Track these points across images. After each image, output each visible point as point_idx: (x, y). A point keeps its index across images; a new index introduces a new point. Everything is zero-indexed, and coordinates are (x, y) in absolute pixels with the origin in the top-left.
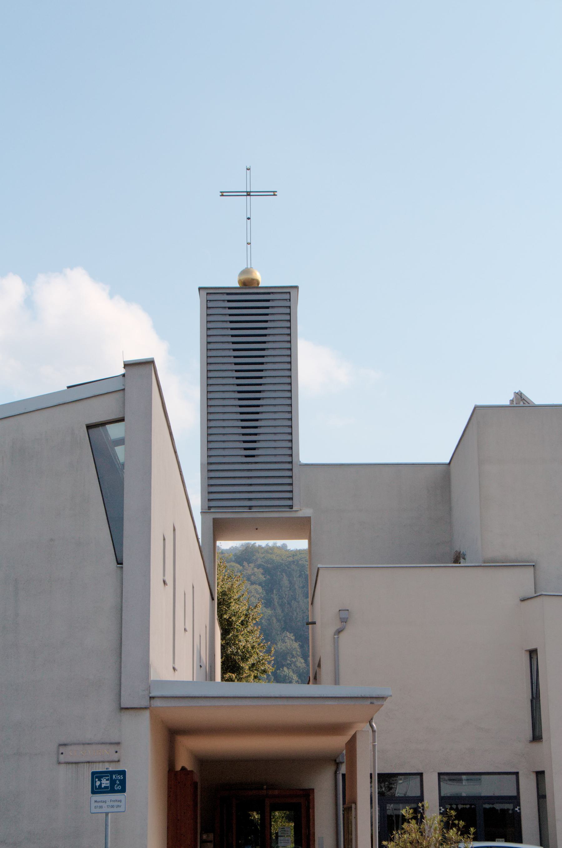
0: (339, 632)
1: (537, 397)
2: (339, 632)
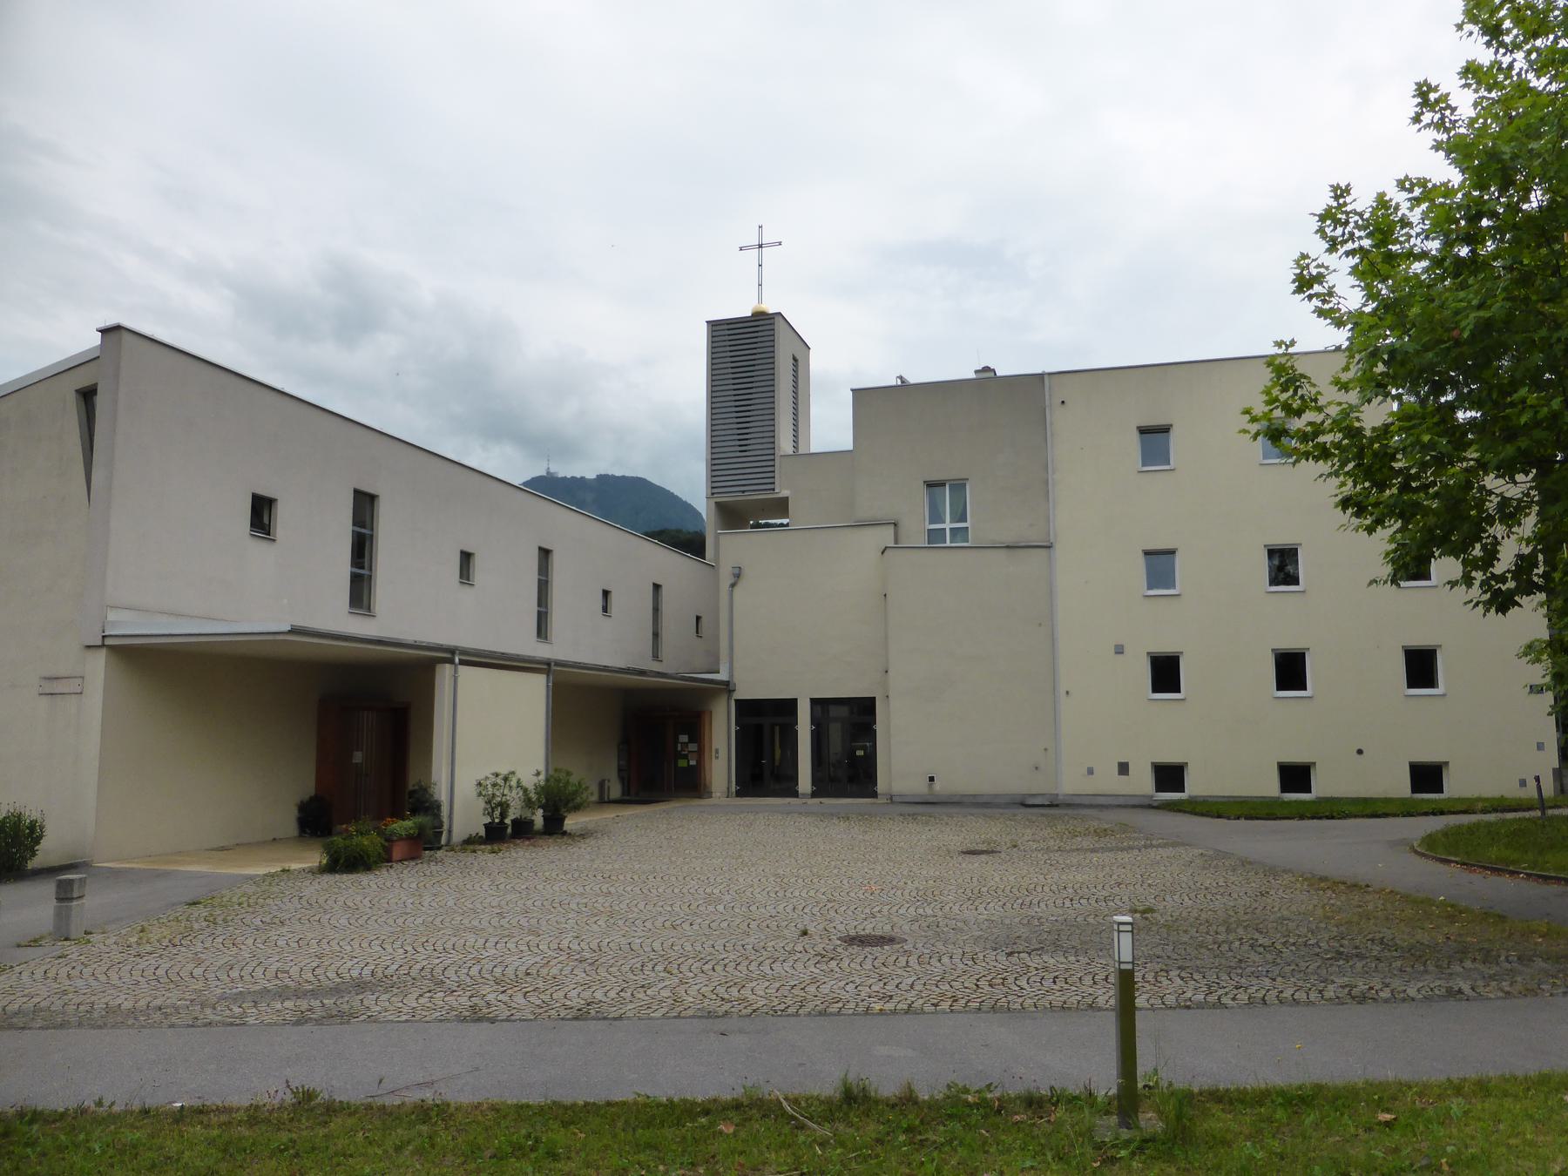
0: (733, 585)
1: (913, 379)
2: (733, 585)
